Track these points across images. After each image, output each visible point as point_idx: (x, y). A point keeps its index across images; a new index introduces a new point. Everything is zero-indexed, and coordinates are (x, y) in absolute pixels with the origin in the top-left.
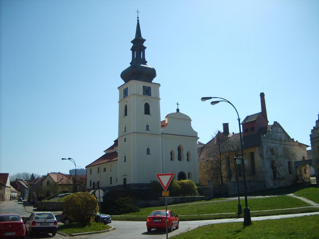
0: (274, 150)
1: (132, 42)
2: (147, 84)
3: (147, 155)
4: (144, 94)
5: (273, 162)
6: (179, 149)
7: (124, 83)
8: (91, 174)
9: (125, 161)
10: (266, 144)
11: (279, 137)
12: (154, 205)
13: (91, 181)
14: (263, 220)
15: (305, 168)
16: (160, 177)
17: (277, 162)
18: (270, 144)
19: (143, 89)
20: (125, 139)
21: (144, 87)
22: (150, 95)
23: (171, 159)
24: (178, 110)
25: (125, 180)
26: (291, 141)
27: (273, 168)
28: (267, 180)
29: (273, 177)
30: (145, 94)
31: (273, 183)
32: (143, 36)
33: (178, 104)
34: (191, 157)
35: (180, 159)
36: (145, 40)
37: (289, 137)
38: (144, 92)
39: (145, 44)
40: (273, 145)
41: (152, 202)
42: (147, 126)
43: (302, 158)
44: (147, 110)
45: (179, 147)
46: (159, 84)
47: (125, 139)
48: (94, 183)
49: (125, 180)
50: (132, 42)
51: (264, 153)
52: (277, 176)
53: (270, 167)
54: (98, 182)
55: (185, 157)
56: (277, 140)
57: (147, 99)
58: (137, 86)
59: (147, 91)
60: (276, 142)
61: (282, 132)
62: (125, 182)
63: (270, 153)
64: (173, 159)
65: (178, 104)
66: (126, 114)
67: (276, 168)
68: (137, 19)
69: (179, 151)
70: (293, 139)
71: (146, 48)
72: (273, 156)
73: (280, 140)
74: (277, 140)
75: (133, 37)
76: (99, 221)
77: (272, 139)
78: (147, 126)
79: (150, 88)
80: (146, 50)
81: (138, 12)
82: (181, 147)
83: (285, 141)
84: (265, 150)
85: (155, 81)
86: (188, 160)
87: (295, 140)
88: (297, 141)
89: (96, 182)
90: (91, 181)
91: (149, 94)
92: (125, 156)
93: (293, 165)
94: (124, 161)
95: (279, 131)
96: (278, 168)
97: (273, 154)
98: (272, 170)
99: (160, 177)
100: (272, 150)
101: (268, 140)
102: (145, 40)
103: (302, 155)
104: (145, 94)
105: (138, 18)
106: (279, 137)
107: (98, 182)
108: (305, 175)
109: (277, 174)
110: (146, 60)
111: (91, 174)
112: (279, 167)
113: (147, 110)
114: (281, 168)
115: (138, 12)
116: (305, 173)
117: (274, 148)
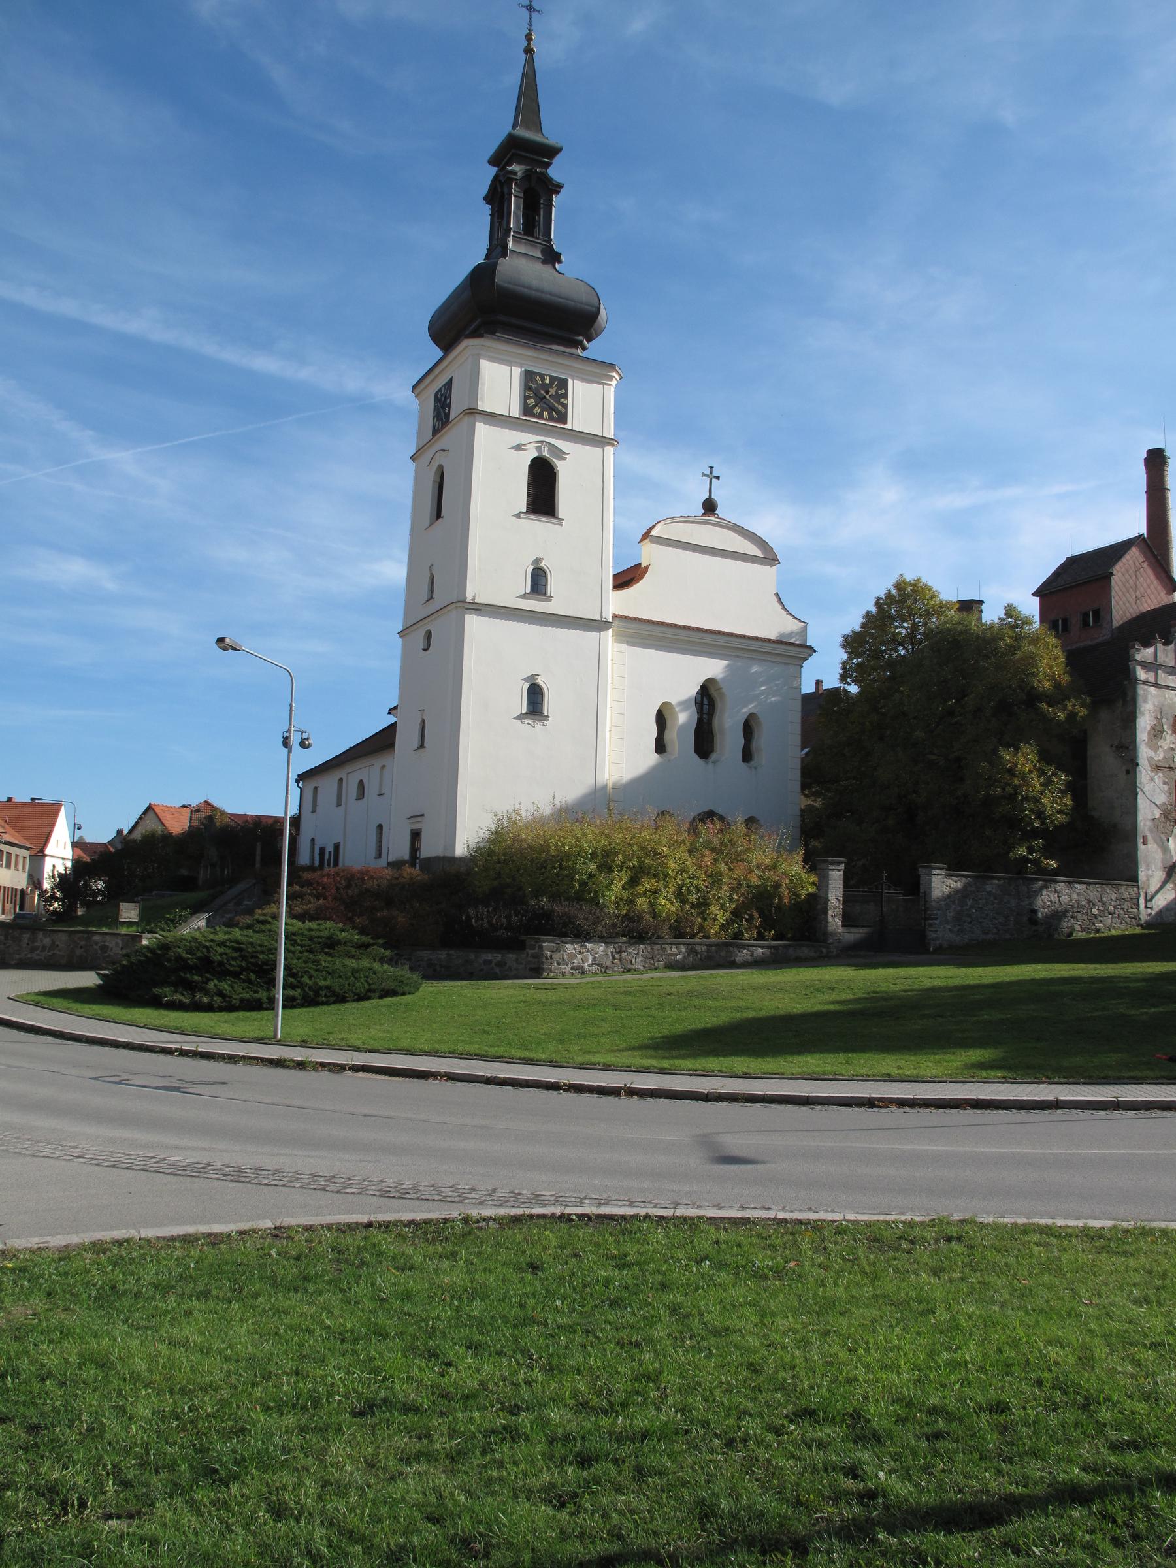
2: (548, 364)
4: (527, 410)
7: (439, 353)
8: (314, 811)
9: (422, 746)
12: (497, 970)
13: (313, 840)
14: (1019, 983)
20: (429, 635)
21: (528, 376)
22: (563, 418)
24: (710, 507)
25: (416, 835)
34: (763, 740)
38: (531, 402)
41: (489, 956)
47: (429, 635)
48: (322, 850)
49: (416, 835)
54: (337, 847)
55: (729, 739)
58: (498, 379)
62: (414, 850)
66: (439, 516)
68: (525, 43)
69: (705, 707)
71: (557, 188)
76: (815, 844)
79: (563, 384)
81: (530, 9)
89: (330, 848)
90: (313, 840)
91: (558, 412)
92: (423, 723)
94: (416, 744)
105: (528, 37)
107: (337, 847)
111: (314, 811)
115: (530, 9)
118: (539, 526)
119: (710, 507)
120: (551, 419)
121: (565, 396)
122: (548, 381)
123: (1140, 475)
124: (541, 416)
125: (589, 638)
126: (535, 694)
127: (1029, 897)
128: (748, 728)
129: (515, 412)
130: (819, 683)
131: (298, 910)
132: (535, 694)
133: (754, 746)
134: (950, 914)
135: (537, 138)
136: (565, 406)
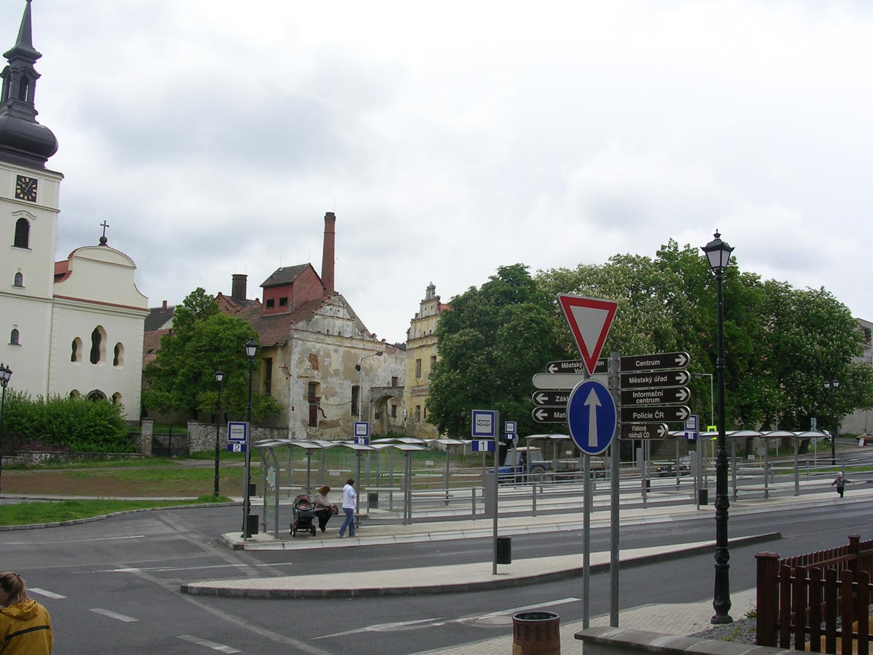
0: (319, 358)
1: (5, 56)
2: (29, 174)
3: (14, 347)
4: (17, 196)
5: (313, 386)
6: (97, 336)
10: (300, 342)
11: (337, 329)
15: (394, 403)
16: (574, 309)
17: (323, 386)
18: (309, 345)
19: (18, 184)
21: (19, 178)
22: (34, 200)
23: (74, 358)
24: (103, 241)
26: (368, 339)
27: (313, 399)
28: (291, 425)
29: (308, 420)
30: (21, 196)
31: (308, 434)
32: (37, 44)
33: (105, 225)
34: (124, 355)
35: (95, 357)
36: (39, 56)
37: (364, 330)
38: (19, 191)
39: (38, 66)
40: (318, 346)
42: (19, 276)
43: (391, 381)
44: (22, 234)
45: (96, 330)
46: (60, 174)
50: (5, 56)
51: (293, 363)
52: (320, 418)
53: (304, 397)
56: (332, 335)
57: (24, 210)
59: (27, 190)
60: (329, 340)
61: (348, 317)
63: (308, 364)
64: (78, 358)
65: (105, 225)
67: (318, 399)
70: (374, 335)
72: (316, 372)
73: (340, 335)
74: (332, 335)
75: (11, 44)
77: (319, 332)
78: (19, 276)
79: (35, 182)
80: (38, 81)
82: (100, 332)
83: (351, 337)
84: (295, 357)
85: (51, 164)
86: (116, 363)
87: (379, 339)
88: (383, 340)
93: (364, 394)
95: (340, 315)
96: (323, 400)
97: (316, 368)
98: (308, 404)
99: (574, 309)
100: (314, 359)
101: (306, 334)
102: (39, 56)
103: (392, 372)
104: (21, 196)
106: (337, 329)
108: (391, 419)
109: (319, 413)
110: (36, 108)
112: (327, 398)
113: (22, 234)
114: (332, 401)
116: (394, 415)
117: (322, 353)
118: (20, 251)
119: (103, 241)
120: (28, 199)
121: (36, 188)
122: (27, 180)
123: (321, 225)
124: (23, 199)
125: (40, 305)
126: (15, 334)
127: (841, 412)
128: (117, 349)
129: (12, 196)
130: (165, 302)
131: (285, 431)
132: (15, 334)
133: (119, 357)
134: (200, 442)
135: (27, 49)
136: (35, 193)
